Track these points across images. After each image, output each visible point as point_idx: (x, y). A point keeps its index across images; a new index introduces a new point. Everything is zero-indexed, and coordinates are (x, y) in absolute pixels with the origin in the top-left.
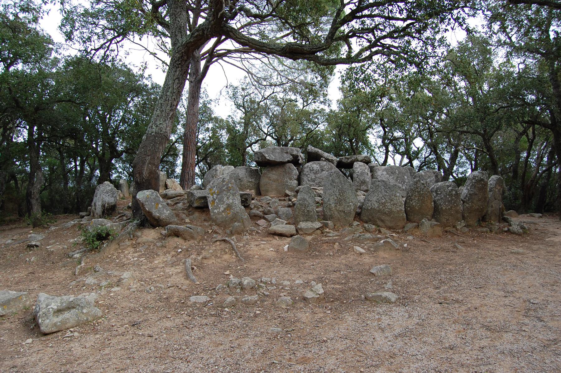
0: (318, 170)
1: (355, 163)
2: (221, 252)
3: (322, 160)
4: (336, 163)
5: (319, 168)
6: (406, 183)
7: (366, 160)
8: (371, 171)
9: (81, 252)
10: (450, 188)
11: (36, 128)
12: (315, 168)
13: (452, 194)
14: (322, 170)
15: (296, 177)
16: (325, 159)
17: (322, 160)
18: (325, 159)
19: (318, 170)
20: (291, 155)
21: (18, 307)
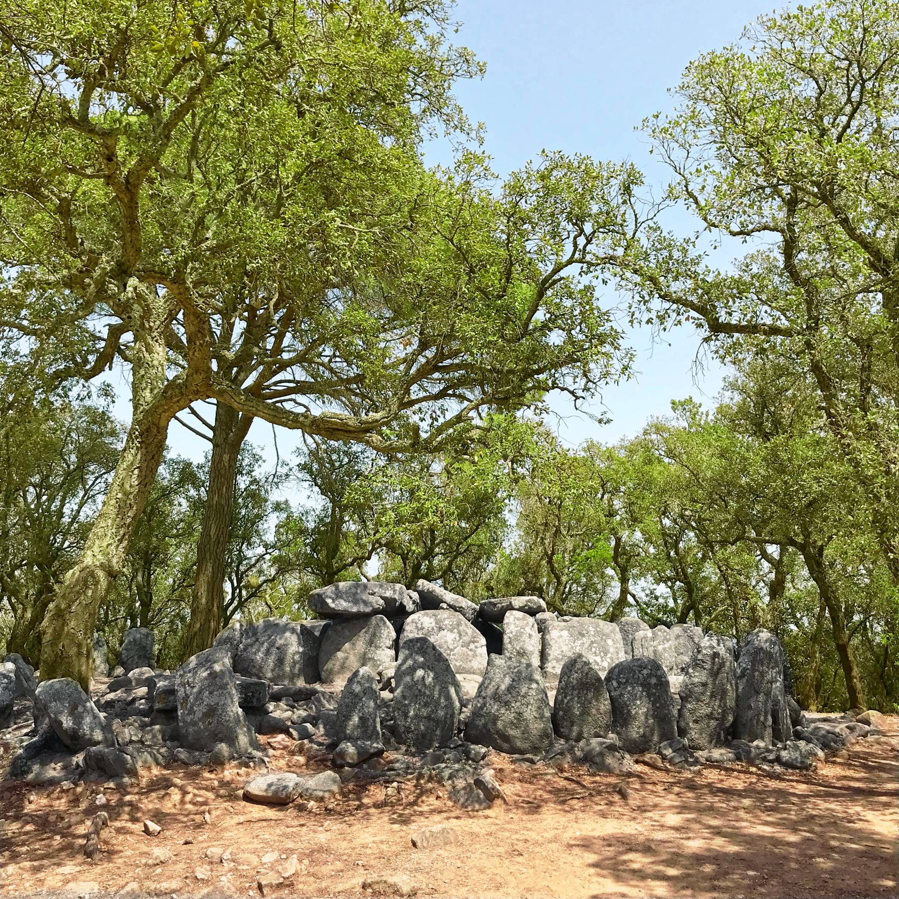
0: (433, 629)
1: (507, 614)
2: (881, 514)
3: (443, 608)
4: (470, 614)
5: (434, 624)
6: (609, 655)
7: (530, 608)
8: (540, 630)
9: (446, 718)
10: (645, 672)
11: (890, 883)
12: (426, 625)
13: (649, 684)
14: (440, 629)
15: (389, 643)
16: (448, 605)
17: (443, 608)
18: (448, 605)
19: (433, 629)
20: (382, 598)
21: (547, 680)
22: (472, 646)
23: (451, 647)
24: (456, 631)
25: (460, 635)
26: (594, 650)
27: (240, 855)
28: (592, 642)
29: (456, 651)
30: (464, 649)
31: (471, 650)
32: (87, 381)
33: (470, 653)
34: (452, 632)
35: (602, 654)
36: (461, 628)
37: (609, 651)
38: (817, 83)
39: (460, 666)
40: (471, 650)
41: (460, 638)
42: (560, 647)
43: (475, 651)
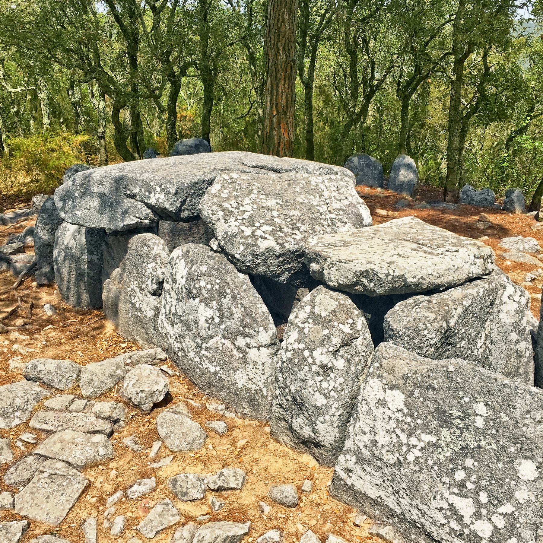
1: (319, 287)
6: (507, 508)
22: (241, 342)
23: (204, 333)
24: (214, 304)
25: (221, 316)
26: (460, 475)
27: (481, 295)
28: (465, 451)
29: (211, 343)
30: (227, 343)
31: (239, 348)
32: (141, 479)
33: (237, 355)
34: (207, 305)
35: (483, 498)
36: (225, 301)
37: (510, 496)
38: (429, 41)
39: (216, 373)
40: (239, 348)
41: (222, 322)
42: (373, 431)
43: (245, 353)
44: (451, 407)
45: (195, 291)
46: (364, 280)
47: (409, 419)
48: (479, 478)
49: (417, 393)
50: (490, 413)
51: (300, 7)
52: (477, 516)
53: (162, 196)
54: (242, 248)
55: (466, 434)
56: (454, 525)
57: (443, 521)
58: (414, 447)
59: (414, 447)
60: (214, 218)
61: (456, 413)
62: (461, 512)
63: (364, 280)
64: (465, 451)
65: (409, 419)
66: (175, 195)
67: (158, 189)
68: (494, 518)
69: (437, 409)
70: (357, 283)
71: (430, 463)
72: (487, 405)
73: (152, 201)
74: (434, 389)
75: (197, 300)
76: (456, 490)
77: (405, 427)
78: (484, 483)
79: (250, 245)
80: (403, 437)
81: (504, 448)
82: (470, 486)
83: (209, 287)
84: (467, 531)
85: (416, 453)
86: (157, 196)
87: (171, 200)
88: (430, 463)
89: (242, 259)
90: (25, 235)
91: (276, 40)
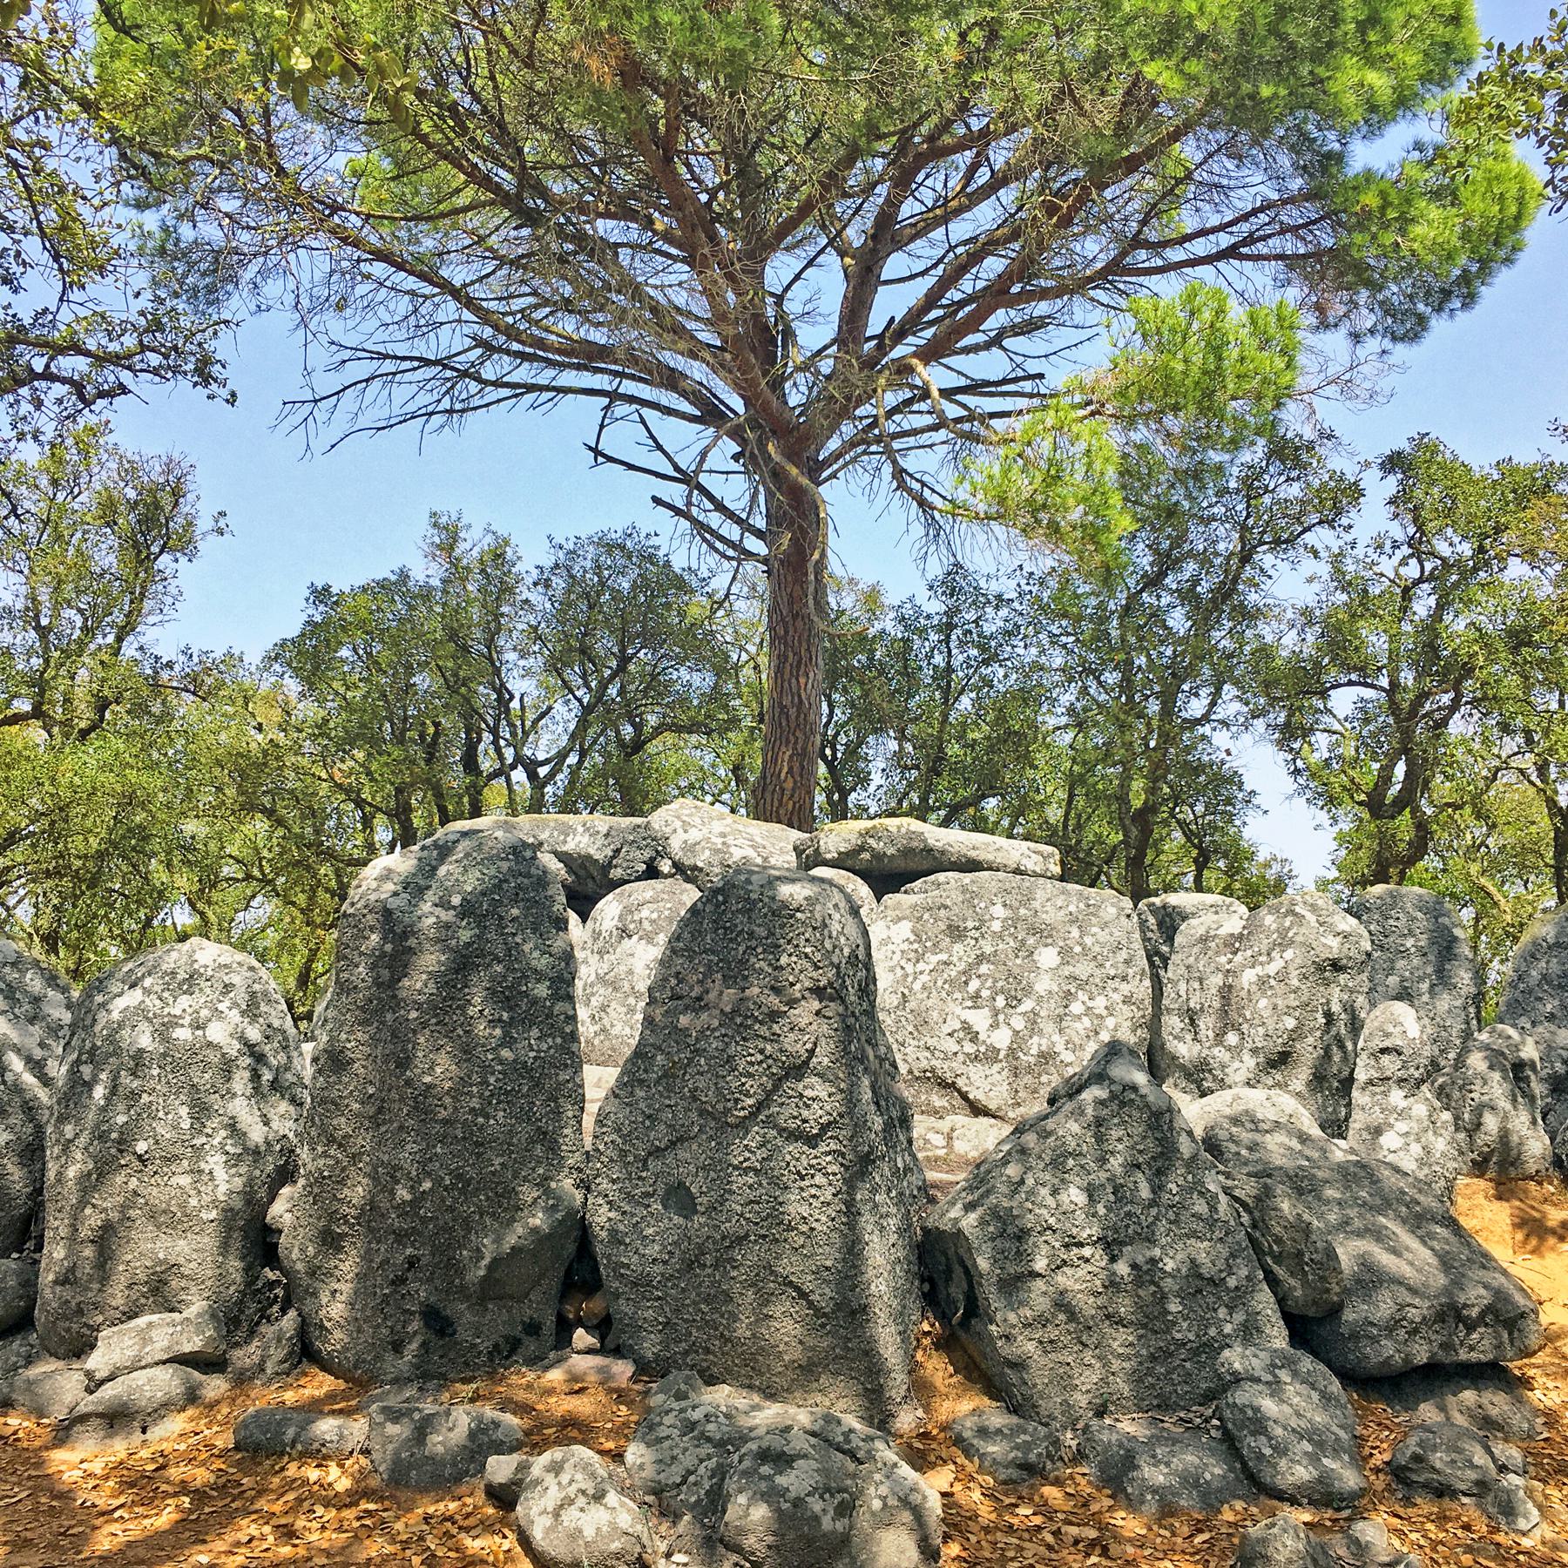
26: (974, 985)
28: (981, 958)
44: (965, 920)
45: (632, 926)
46: (871, 841)
47: (916, 946)
48: (995, 981)
49: (926, 916)
50: (1009, 913)
51: (824, 757)
52: (994, 1026)
53: (585, 839)
54: (707, 853)
55: (981, 942)
56: (969, 1048)
57: (956, 1048)
58: (921, 973)
59: (921, 973)
60: (668, 830)
61: (970, 924)
62: (976, 1028)
63: (871, 841)
64: (981, 958)
65: (916, 946)
66: (607, 835)
67: (580, 829)
68: (1013, 1022)
69: (949, 927)
70: (862, 848)
71: (940, 983)
72: (1005, 905)
73: (570, 846)
74: (946, 907)
75: (635, 938)
76: (969, 1003)
77: (912, 955)
78: (1000, 984)
79: (717, 851)
80: (909, 968)
81: (1023, 942)
82: (985, 993)
83: (655, 916)
84: (983, 1049)
85: (925, 978)
86: (578, 838)
87: (599, 844)
88: (940, 983)
89: (707, 869)
90: (297, 1027)
91: (776, 803)
